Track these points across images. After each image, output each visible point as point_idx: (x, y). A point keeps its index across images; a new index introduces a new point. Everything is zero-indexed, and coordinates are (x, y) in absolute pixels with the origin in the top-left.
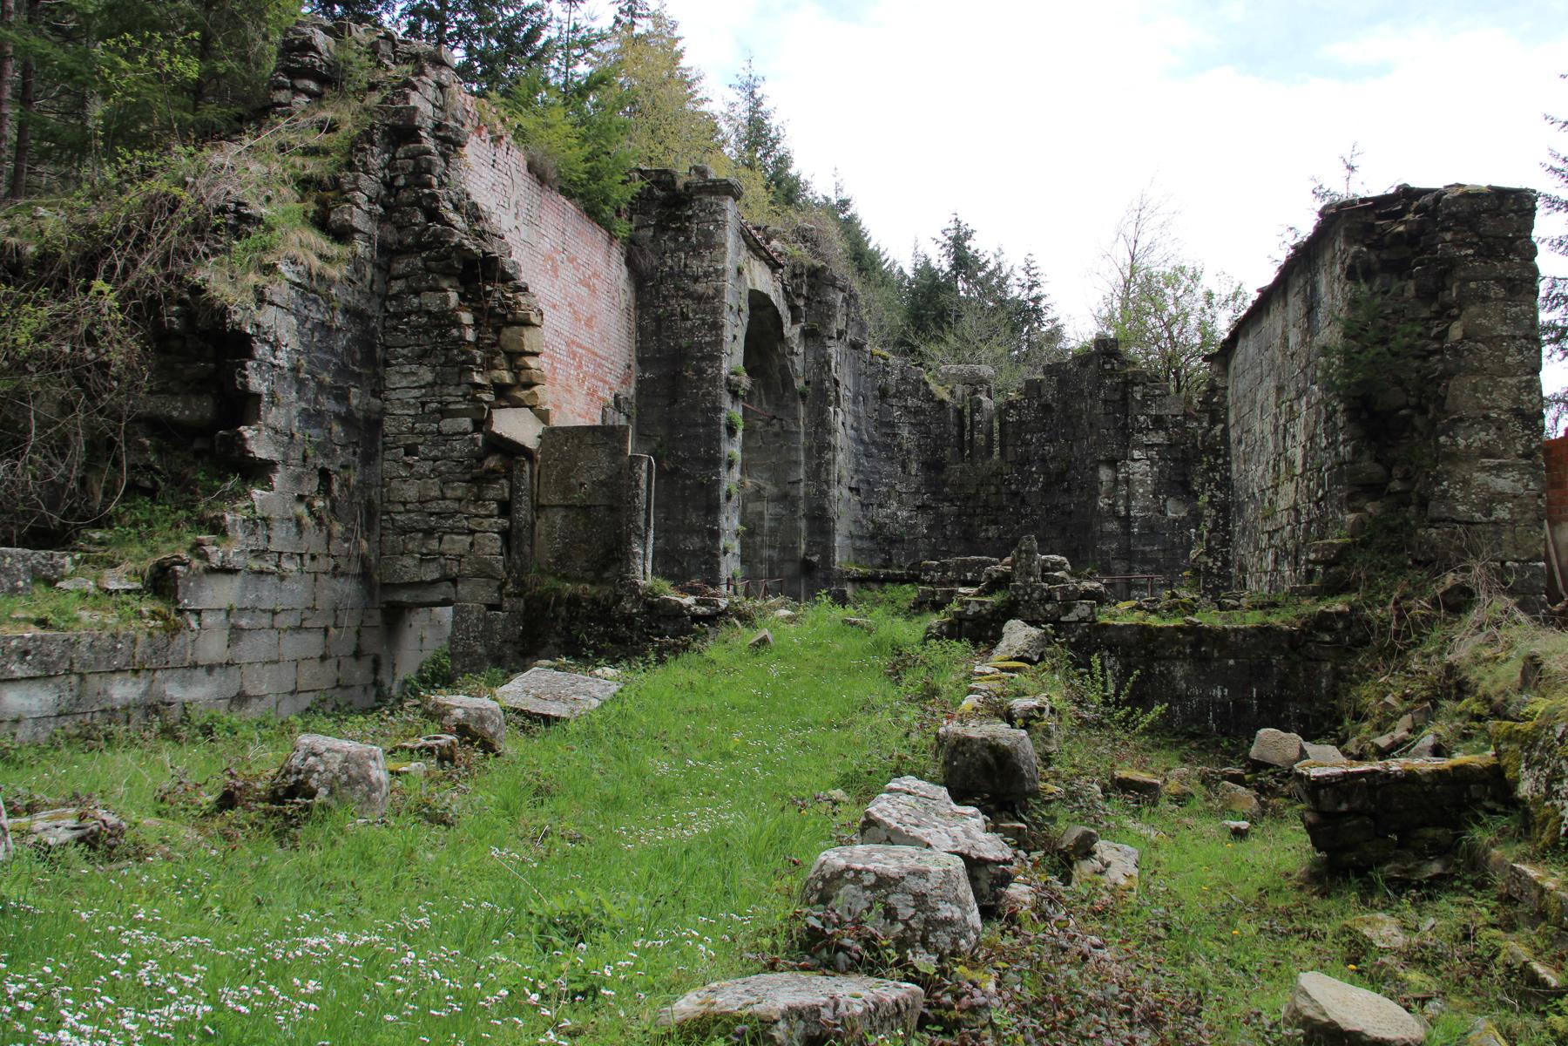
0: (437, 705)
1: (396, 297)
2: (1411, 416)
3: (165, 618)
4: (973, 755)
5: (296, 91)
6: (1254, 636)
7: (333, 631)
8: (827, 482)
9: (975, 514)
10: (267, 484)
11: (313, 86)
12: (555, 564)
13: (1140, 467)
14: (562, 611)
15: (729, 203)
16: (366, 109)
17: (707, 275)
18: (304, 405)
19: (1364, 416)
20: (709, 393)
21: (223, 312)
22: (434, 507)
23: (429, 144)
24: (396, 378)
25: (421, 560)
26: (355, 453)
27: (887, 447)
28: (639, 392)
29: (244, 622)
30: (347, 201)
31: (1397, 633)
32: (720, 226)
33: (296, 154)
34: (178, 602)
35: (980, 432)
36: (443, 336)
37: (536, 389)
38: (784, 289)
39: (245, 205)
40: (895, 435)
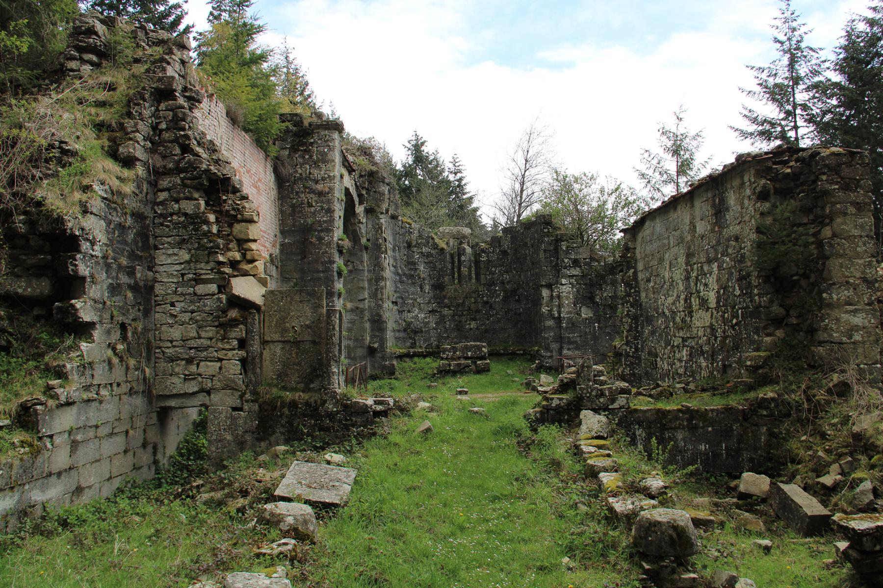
0: (272, 514)
1: (162, 203)
2: (798, 280)
3: (31, 445)
4: (662, 533)
5: (83, 61)
6: (723, 413)
7: (131, 432)
8: (381, 300)
9: (463, 315)
10: (89, 338)
11: (94, 58)
12: (277, 379)
13: (566, 289)
14: (286, 411)
15: (336, 135)
16: (134, 76)
17: (323, 179)
18: (110, 281)
19: (772, 280)
20: (326, 252)
21: (60, 220)
22: (192, 343)
23: (181, 101)
24: (163, 257)
25: (185, 379)
26: (139, 310)
27: (411, 277)
28: (282, 251)
29: (79, 437)
30: (131, 139)
31: (809, 410)
32: (331, 149)
33: (91, 106)
34: (39, 432)
35: (465, 267)
36: (196, 230)
37: (256, 263)
38: (356, 184)
39: (66, 143)
40: (416, 269)
